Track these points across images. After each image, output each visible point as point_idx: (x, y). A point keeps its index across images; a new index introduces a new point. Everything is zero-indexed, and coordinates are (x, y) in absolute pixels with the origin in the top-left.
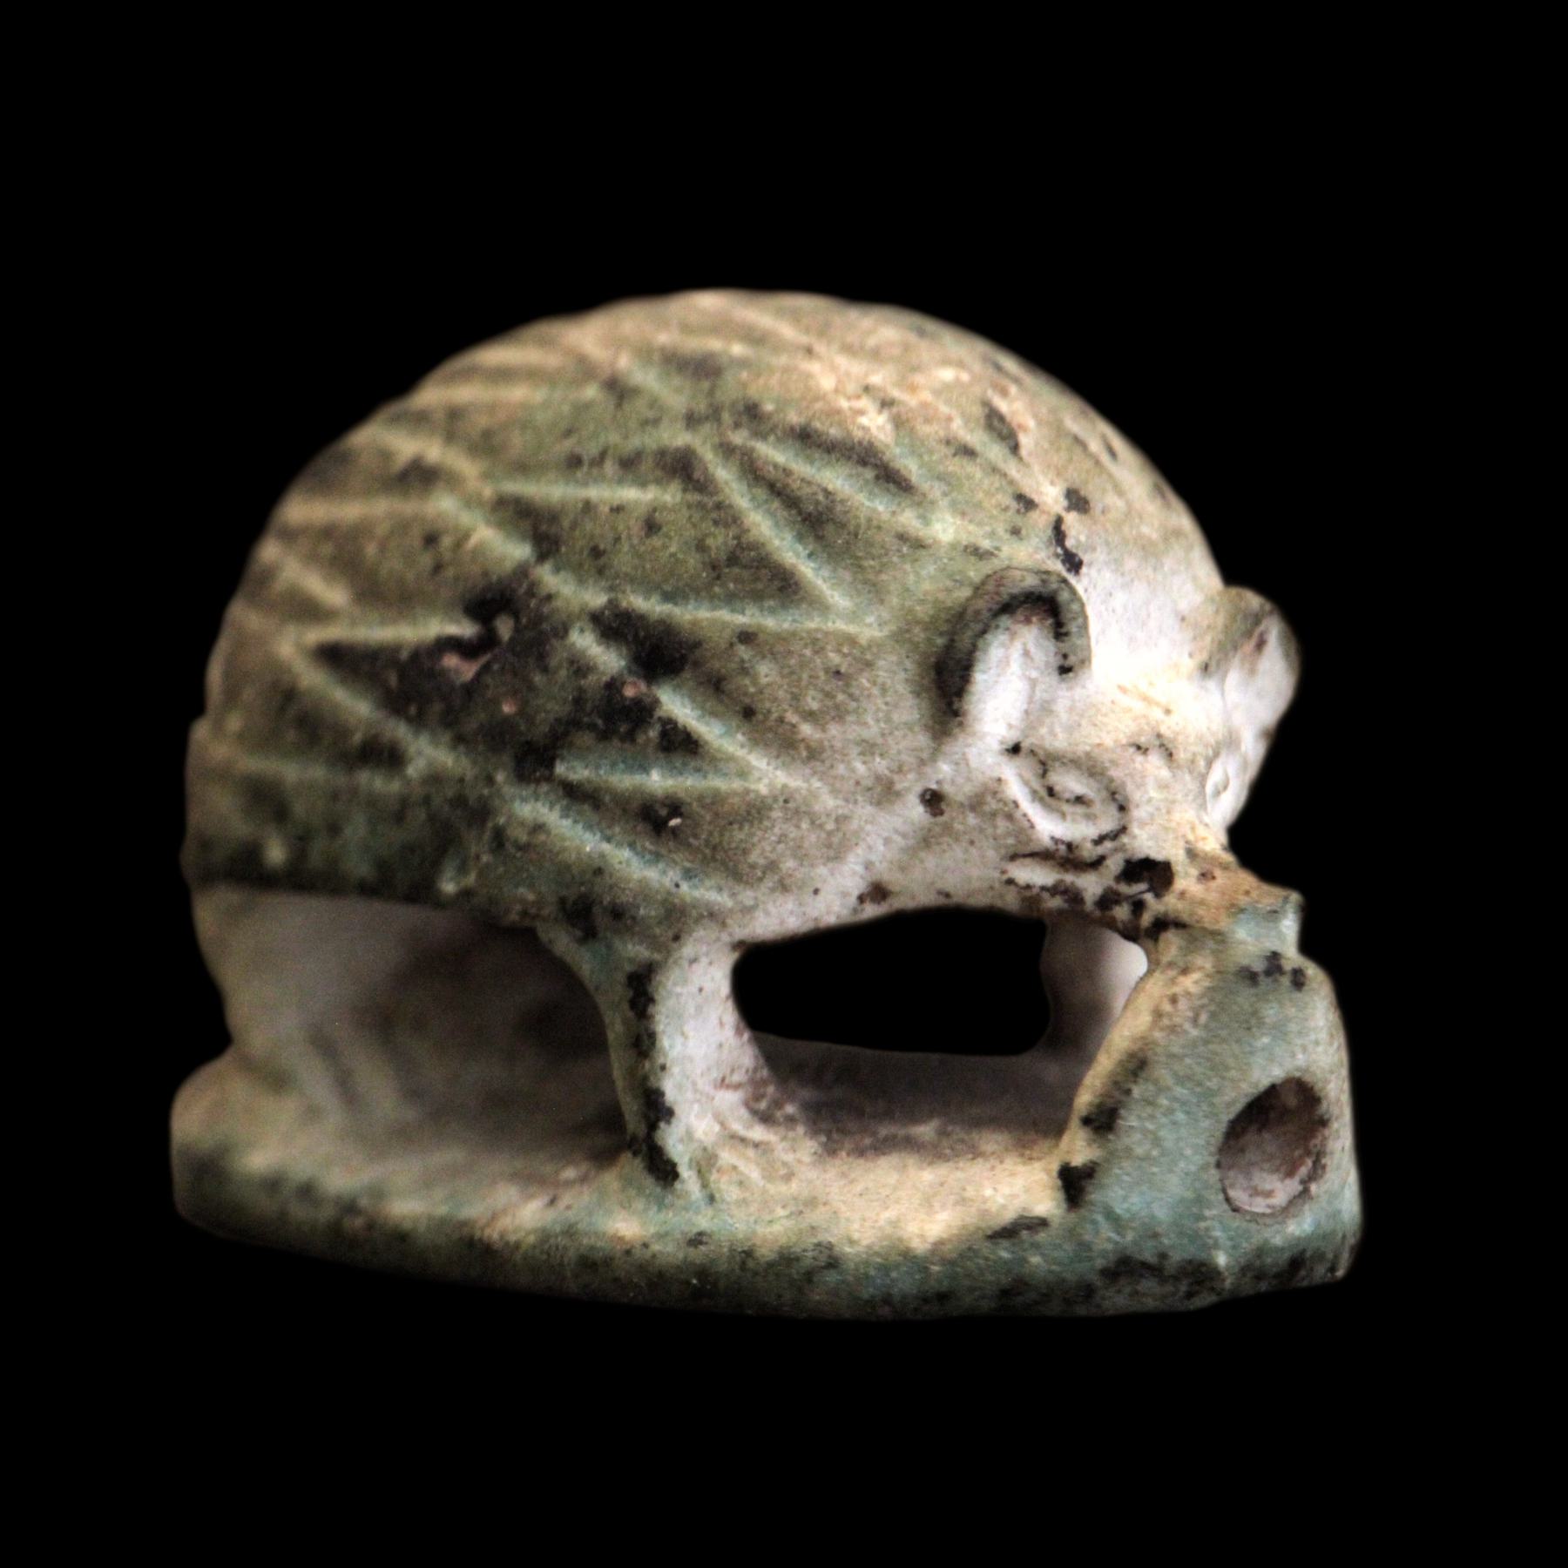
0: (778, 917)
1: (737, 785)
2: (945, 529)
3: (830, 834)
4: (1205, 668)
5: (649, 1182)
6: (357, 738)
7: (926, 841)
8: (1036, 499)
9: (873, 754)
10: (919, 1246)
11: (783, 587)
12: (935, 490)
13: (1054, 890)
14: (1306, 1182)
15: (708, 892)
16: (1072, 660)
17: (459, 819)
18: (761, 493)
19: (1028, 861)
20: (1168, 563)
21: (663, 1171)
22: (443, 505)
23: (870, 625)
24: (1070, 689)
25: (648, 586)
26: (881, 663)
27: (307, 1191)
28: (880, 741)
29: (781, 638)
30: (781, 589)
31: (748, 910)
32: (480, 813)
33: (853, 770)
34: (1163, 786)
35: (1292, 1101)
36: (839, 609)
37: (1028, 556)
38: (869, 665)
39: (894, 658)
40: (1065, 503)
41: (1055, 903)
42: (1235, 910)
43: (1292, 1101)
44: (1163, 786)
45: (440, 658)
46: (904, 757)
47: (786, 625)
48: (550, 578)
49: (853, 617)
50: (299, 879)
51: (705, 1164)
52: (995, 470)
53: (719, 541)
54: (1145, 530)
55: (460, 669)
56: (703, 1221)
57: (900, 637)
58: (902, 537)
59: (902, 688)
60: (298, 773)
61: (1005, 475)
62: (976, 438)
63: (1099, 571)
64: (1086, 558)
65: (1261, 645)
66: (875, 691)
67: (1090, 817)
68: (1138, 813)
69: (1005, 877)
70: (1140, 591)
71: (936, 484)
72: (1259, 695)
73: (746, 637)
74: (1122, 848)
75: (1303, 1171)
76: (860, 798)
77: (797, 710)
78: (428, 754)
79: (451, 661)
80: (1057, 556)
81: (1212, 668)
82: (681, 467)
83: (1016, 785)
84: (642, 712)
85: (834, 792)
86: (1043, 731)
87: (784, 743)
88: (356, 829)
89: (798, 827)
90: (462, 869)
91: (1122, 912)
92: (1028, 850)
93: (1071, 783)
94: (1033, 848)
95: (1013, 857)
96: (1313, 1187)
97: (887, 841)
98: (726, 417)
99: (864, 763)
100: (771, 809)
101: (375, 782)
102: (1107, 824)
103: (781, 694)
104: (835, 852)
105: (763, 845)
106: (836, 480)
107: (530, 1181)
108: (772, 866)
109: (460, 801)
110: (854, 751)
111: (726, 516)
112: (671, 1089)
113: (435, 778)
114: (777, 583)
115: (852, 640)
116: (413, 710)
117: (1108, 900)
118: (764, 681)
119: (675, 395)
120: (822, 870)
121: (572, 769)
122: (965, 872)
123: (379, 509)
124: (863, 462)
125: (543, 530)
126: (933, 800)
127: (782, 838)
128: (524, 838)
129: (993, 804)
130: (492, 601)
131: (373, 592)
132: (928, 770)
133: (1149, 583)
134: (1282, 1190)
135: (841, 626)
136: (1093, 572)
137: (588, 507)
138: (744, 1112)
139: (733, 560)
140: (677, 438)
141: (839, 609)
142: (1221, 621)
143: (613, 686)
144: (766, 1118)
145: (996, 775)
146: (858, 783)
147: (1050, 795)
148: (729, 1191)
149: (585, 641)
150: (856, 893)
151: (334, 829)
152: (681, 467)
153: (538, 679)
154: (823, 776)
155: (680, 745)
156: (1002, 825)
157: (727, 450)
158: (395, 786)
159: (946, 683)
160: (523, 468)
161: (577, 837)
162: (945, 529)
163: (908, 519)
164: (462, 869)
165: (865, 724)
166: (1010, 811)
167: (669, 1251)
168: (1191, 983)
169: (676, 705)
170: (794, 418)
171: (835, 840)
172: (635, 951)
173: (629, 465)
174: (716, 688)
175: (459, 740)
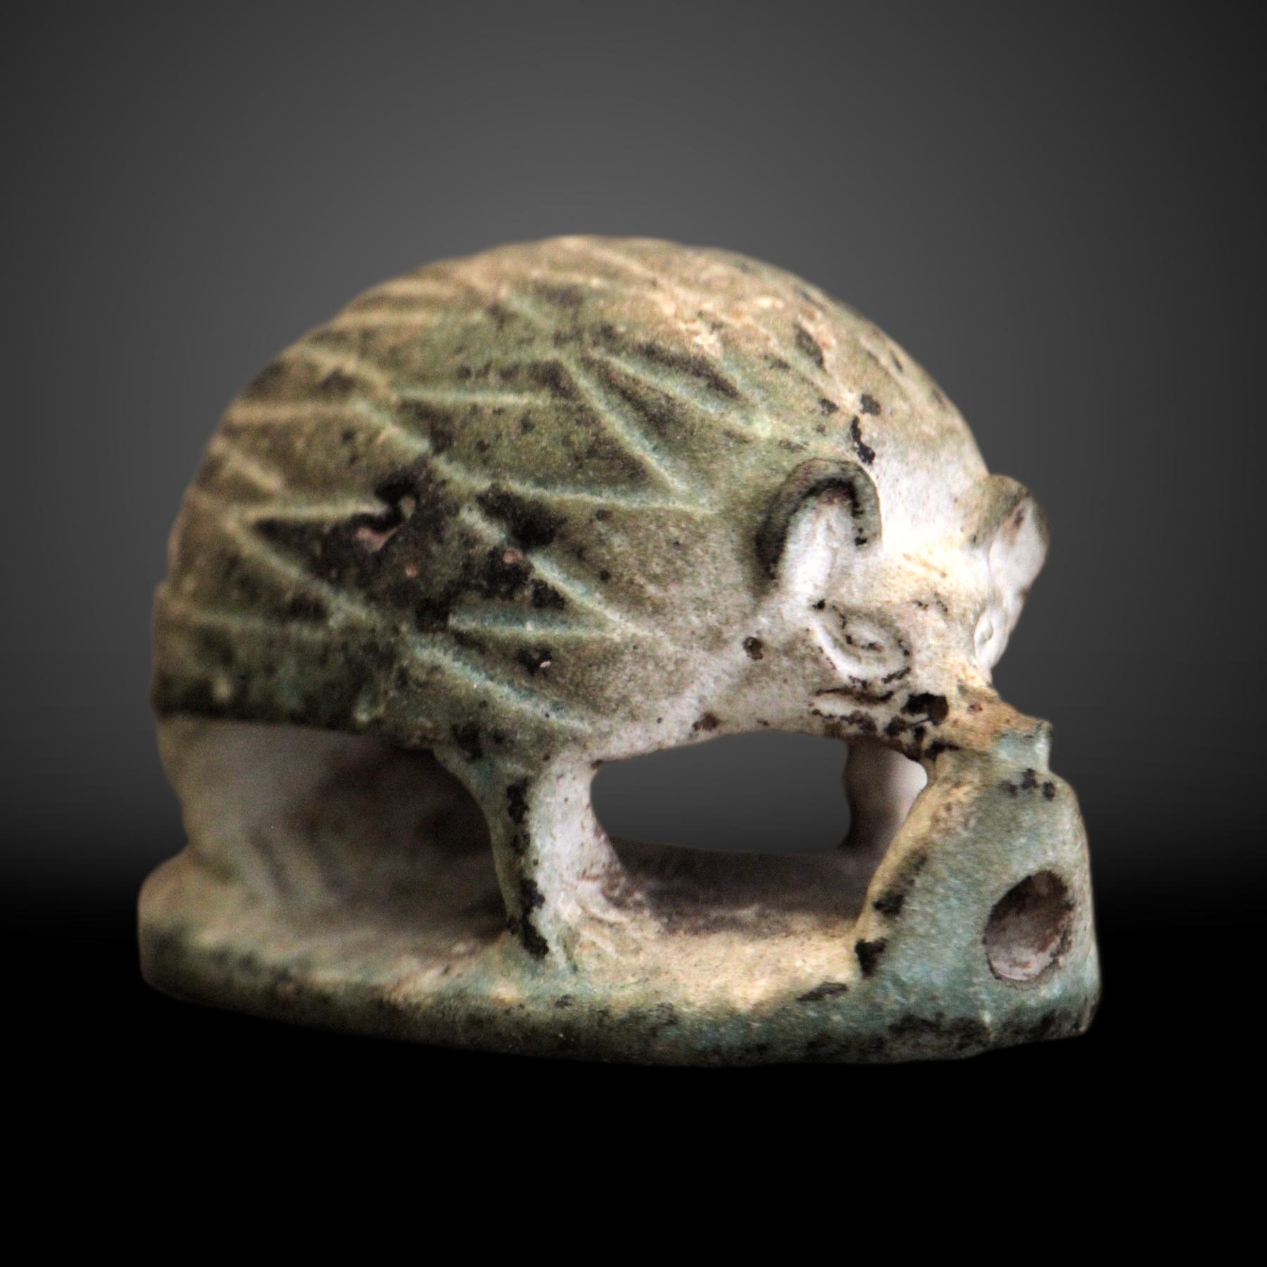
0: (628, 740)
1: (595, 634)
2: (764, 427)
3: (670, 674)
4: (974, 540)
5: (524, 955)
6: (289, 596)
7: (748, 679)
8: (837, 403)
9: (705, 609)
10: (743, 1007)
11: (633, 474)
12: (755, 396)
13: (852, 719)
14: (1055, 955)
15: (572, 721)
16: (866, 533)
17: (371, 661)
18: (615, 398)
19: (830, 696)
20: (944, 455)
21: (536, 946)
22: (358, 408)
23: (703, 505)
24: (865, 556)
25: (524, 473)
26: (712, 536)
27: (248, 963)
28: (711, 598)
29: (631, 515)
30: (631, 476)
31: (604, 736)
32: (388, 657)
33: (689, 623)
34: (940, 635)
35: (1044, 890)
36: (678, 492)
37: (831, 450)
38: (702, 537)
39: (722, 532)
40: (860, 406)
41: (853, 729)
42: (998, 735)
43: (1044, 890)
44: (940, 635)
46: (731, 612)
47: (635, 505)
48: (444, 467)
49: (690, 498)
50: (242, 710)
51: (570, 941)
52: (804, 380)
53: (581, 437)
54: (925, 428)
55: (372, 540)
56: (568, 987)
57: (727, 514)
58: (729, 434)
59: (729, 556)
60: (241, 625)
61: (812, 384)
62: (789, 354)
63: (888, 461)
64: (877, 451)
65: (1019, 521)
66: (707, 558)
67: (881, 660)
68: (920, 657)
69: (812, 709)
70: (921, 477)
71: (757, 391)
72: (1017, 562)
73: (603, 515)
74: (907, 686)
75: (1053, 946)
76: (695, 645)
77: (644, 574)
78: (346, 609)
79: (364, 534)
80: (854, 449)
81: (980, 539)
82: (550, 377)
83: (821, 634)
84: (518, 576)
85: (674, 640)
86: (843, 590)
87: (634, 601)
88: (288, 670)
89: (645, 668)
90: (374, 702)
91: (906, 737)
92: (831, 687)
93: (865, 633)
94: (834, 685)
95: (819, 693)
96: (1061, 960)
97: (717, 680)
98: (587, 337)
99: (698, 616)
100: (623, 653)
101: (303, 632)
102: (894, 666)
103: (631, 561)
104: (675, 688)
105: (616, 683)
106: (676, 388)
107: (428, 954)
108: (624, 700)
109: (371, 647)
110: (690, 607)
111: (586, 417)
112: (542, 880)
113: (351, 629)
114: (628, 471)
115: (688, 518)
116: (334, 574)
117: (895, 727)
118: (617, 550)
119: (545, 319)
120: (664, 703)
121: (462, 622)
122: (781, 701)
123: (307, 411)
124: (697, 373)
125: (439, 428)
126: (754, 646)
127: (632, 677)
128: (423, 677)
129: (802, 650)
130: (398, 485)
132: (750, 622)
133: (928, 471)
134: (1036, 961)
135: (679, 505)
136: (883, 462)
137: (475, 410)
138: (601, 899)
139: (592, 452)
140: (547, 354)
141: (678, 492)
142: (986, 502)
143: (496, 554)
144: (619, 904)
145: (804, 626)
146: (693, 633)
147: (848, 643)
148: (589, 962)
149: (472, 518)
150: (692, 722)
151: (270, 670)
152: (550, 377)
153: (435, 548)
154: (665, 627)
155: (549, 602)
156: (810, 666)
157: (587, 364)
158: (319, 635)
159: (765, 552)
160: (422, 378)
161: (466, 676)
162: (764, 427)
163: (734, 419)
164: (374, 702)
165: (699, 585)
166: (816, 656)
167: (541, 1011)
168: (962, 794)
169: (546, 569)
170: (641, 338)
171: (675, 679)
172: (513, 768)
173: (508, 376)
174: (578, 556)
175: (371, 598)
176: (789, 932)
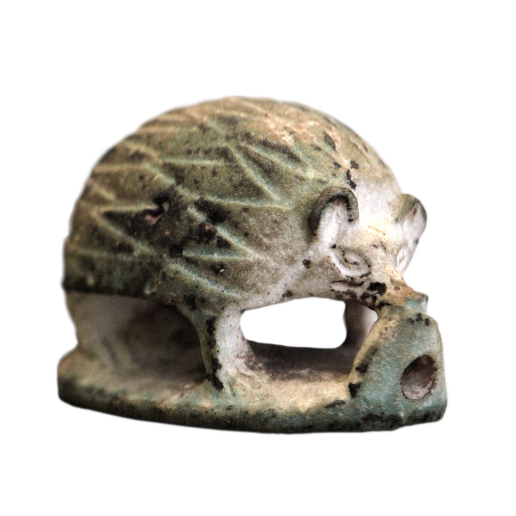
1: (242, 258)
2: (311, 174)
3: (273, 274)
4: (397, 220)
5: (214, 389)
6: (118, 243)
7: (305, 277)
8: (341, 164)
9: (287, 248)
10: (302, 410)
11: (258, 193)
12: (308, 161)
14: (430, 389)
16: (353, 217)
17: (151, 269)
18: (251, 162)
19: (338, 283)
20: (384, 185)
21: (218, 385)
22: (146, 166)
23: (286, 206)
24: (352, 227)
25: (213, 193)
26: (290, 218)
28: (289, 244)
29: (257, 210)
30: (257, 194)
31: (246, 300)
32: (158, 268)
33: (281, 254)
34: (383, 259)
35: (425, 362)
36: (276, 201)
37: (338, 183)
38: (286, 219)
39: (294, 217)
40: (350, 166)
43: (425, 362)
44: (383, 259)
45: (145, 217)
46: (298, 249)
47: (259, 206)
48: (181, 190)
49: (281, 203)
51: (232, 383)
53: (237, 178)
54: (377, 174)
55: (151, 220)
56: (231, 402)
57: (296, 209)
58: (297, 177)
59: (297, 226)
61: (331, 156)
62: (321, 144)
63: (362, 188)
64: (357, 184)
66: (288, 227)
67: (359, 269)
68: (375, 268)
69: (331, 289)
70: (375, 194)
71: (308, 159)
72: (414, 229)
73: (246, 210)
74: (369, 279)
75: (429, 385)
76: (283, 263)
77: (262, 234)
78: (141, 248)
79: (148, 218)
80: (348, 183)
81: (399, 220)
82: (224, 154)
83: (334, 258)
84: (211, 234)
85: (275, 261)
86: (343, 240)
87: (258, 245)
88: (117, 273)
89: (263, 272)
90: (152, 286)
91: (369, 300)
92: (338, 280)
93: (352, 258)
94: (340, 279)
95: (333, 282)
96: (432, 391)
97: (292, 277)
98: (239, 137)
99: (284, 251)
100: (254, 266)
101: (123, 257)
102: (364, 271)
103: (257, 228)
104: (275, 280)
105: (251, 278)
106: (275, 158)
107: (174, 389)
108: (254, 285)
109: (151, 264)
110: (281, 247)
111: (239, 170)
112: (221, 358)
113: (143, 256)
114: (256, 192)
115: (280, 211)
116: (136, 234)
117: (365, 296)
118: (251, 224)
119: (222, 130)
120: (270, 286)
121: (188, 253)
124: (284, 152)
125: (179, 174)
126: (307, 263)
127: (257, 276)
128: (172, 276)
129: (327, 265)
130: (162, 198)
131: (123, 195)
132: (305, 253)
133: (378, 192)
134: (422, 391)
135: (277, 206)
136: (360, 188)
137: (194, 167)
138: (245, 366)
139: (241, 184)
140: (223, 144)
141: (276, 201)
142: (402, 204)
143: (202, 226)
144: (252, 368)
145: (328, 255)
146: (282, 258)
147: (345, 262)
148: (240, 392)
149: (192, 211)
150: (282, 294)
151: (110, 273)
152: (224, 154)
153: (177, 223)
154: (271, 255)
155: (224, 245)
156: (330, 271)
157: (239, 148)
158: (130, 259)
159: (311, 225)
160: (172, 154)
161: (190, 276)
162: (311, 174)
163: (299, 171)
164: (152, 286)
165: (285, 238)
166: (332, 267)
168: (392, 324)
169: (223, 232)
170: (261, 137)
171: (275, 276)
172: (209, 313)
173: (207, 153)
174: (236, 226)
175: (151, 244)
176: (321, 380)
